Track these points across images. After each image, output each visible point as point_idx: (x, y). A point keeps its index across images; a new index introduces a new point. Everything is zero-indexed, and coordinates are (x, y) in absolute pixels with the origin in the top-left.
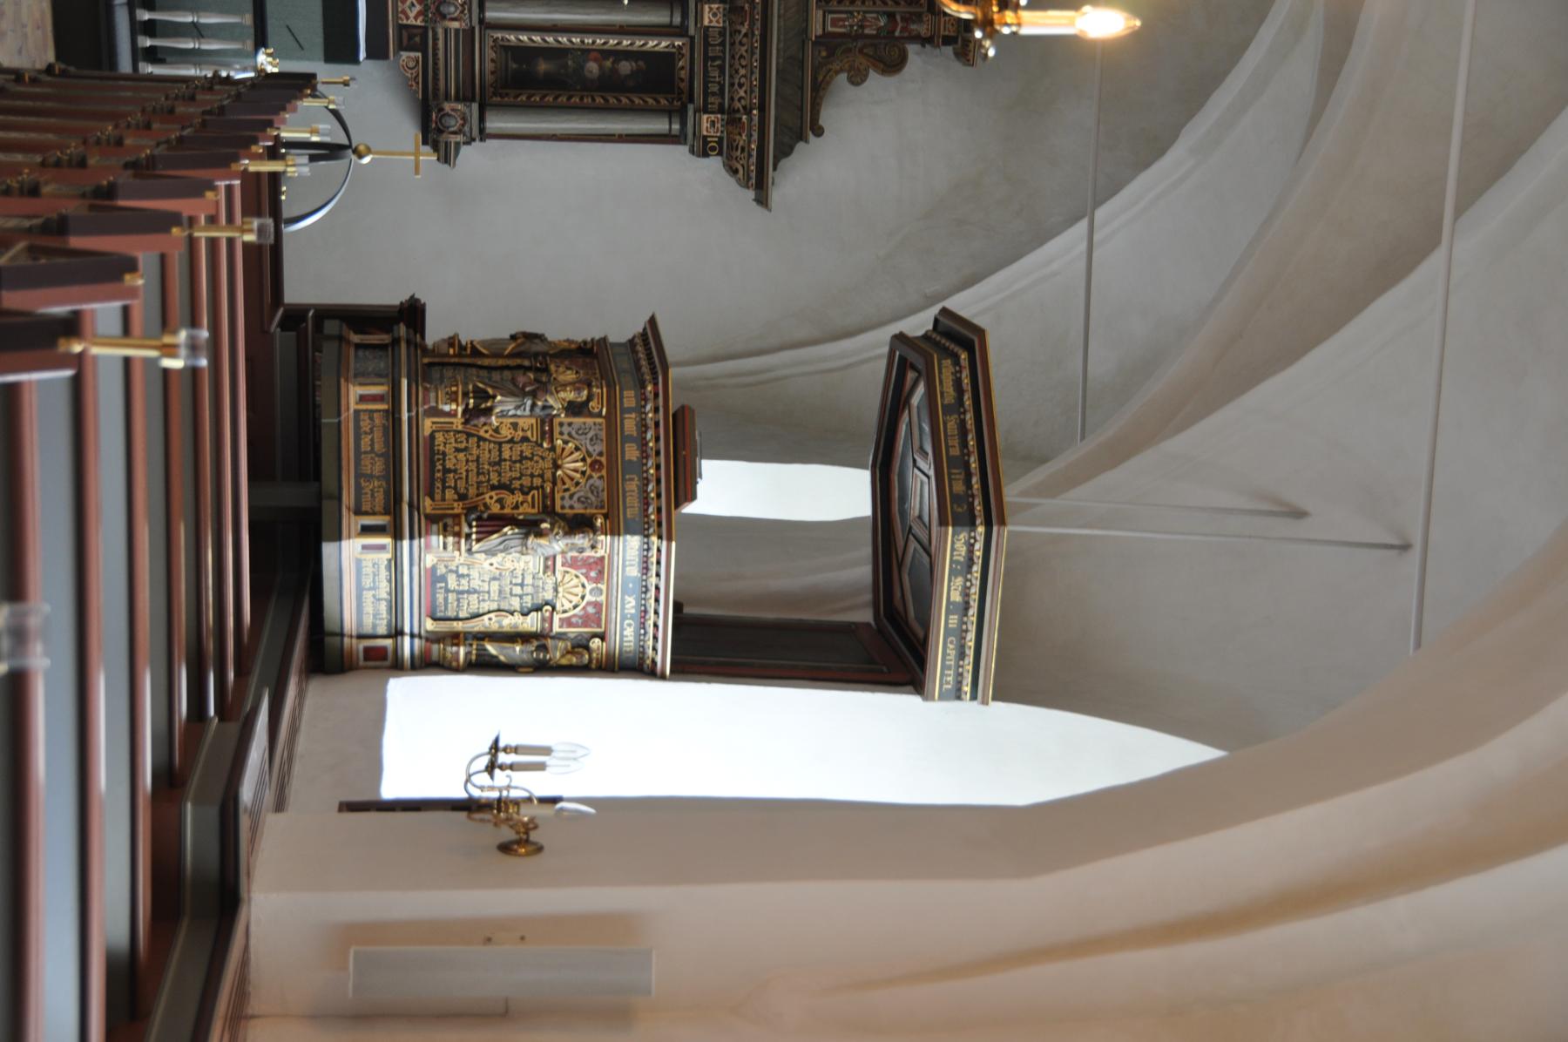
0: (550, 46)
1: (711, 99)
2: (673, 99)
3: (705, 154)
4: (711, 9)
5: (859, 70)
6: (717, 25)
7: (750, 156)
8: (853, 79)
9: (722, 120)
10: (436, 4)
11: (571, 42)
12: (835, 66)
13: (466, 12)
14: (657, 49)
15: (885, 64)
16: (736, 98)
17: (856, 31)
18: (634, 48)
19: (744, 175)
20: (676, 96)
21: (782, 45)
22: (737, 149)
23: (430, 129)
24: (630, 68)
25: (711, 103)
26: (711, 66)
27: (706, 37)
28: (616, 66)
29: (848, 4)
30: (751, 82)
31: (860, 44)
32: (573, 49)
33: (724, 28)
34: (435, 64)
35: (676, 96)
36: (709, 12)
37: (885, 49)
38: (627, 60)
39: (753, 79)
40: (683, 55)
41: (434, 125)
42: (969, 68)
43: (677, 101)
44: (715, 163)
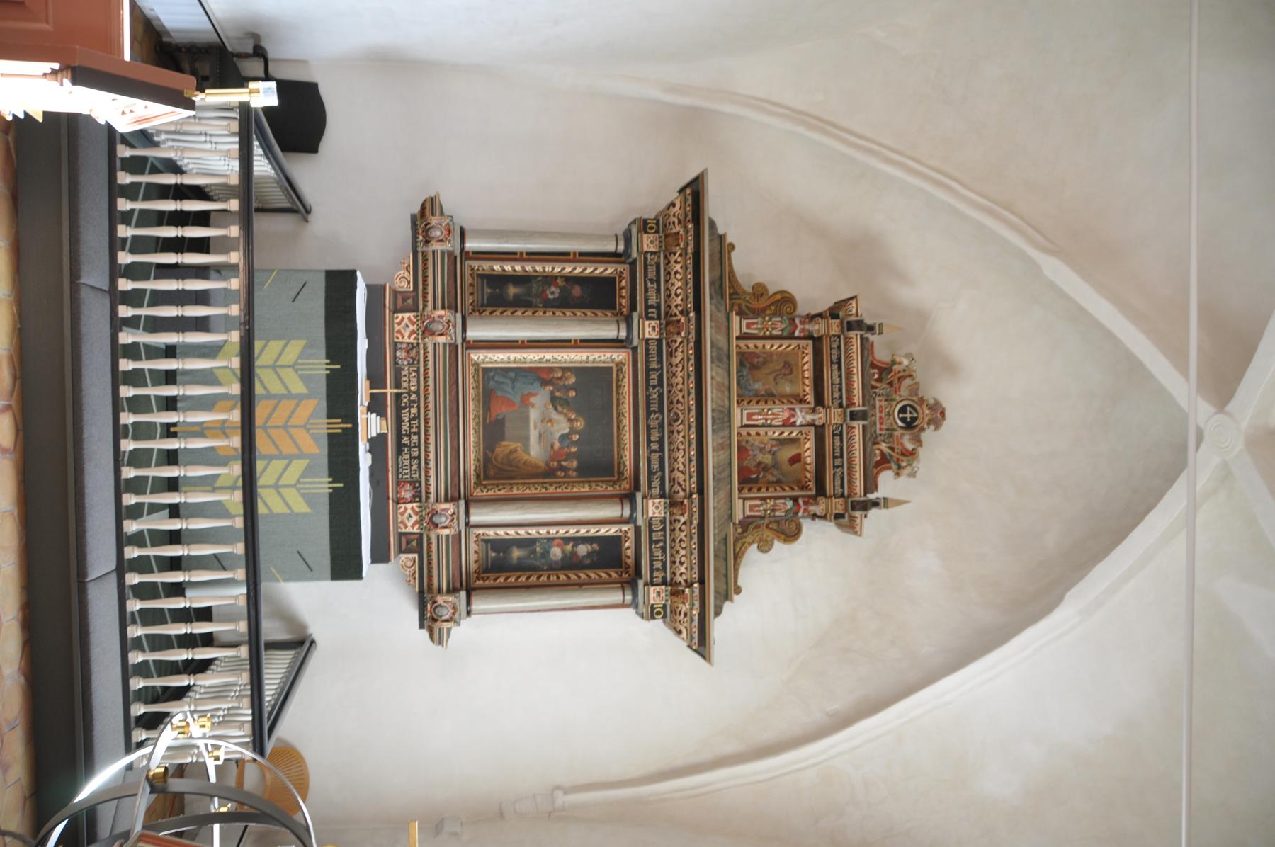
0: (522, 537)
1: (656, 574)
2: (622, 572)
3: (653, 618)
4: (654, 503)
5: (766, 541)
6: (659, 515)
7: (692, 620)
8: (762, 548)
9: (666, 591)
10: (430, 515)
11: (539, 533)
12: (749, 539)
13: (455, 520)
14: (607, 534)
15: (786, 535)
16: (678, 573)
17: (769, 514)
18: (590, 534)
19: (687, 635)
21: (716, 531)
22: (680, 614)
23: (425, 617)
24: (586, 550)
25: (656, 577)
26: (655, 548)
27: (650, 525)
28: (575, 549)
29: (756, 491)
30: (691, 561)
31: (766, 521)
32: (541, 538)
33: (665, 518)
34: (429, 563)
35: (623, 570)
36: (653, 506)
40: (629, 538)
41: (429, 615)
42: (850, 537)
43: (626, 574)
44: (659, 622)
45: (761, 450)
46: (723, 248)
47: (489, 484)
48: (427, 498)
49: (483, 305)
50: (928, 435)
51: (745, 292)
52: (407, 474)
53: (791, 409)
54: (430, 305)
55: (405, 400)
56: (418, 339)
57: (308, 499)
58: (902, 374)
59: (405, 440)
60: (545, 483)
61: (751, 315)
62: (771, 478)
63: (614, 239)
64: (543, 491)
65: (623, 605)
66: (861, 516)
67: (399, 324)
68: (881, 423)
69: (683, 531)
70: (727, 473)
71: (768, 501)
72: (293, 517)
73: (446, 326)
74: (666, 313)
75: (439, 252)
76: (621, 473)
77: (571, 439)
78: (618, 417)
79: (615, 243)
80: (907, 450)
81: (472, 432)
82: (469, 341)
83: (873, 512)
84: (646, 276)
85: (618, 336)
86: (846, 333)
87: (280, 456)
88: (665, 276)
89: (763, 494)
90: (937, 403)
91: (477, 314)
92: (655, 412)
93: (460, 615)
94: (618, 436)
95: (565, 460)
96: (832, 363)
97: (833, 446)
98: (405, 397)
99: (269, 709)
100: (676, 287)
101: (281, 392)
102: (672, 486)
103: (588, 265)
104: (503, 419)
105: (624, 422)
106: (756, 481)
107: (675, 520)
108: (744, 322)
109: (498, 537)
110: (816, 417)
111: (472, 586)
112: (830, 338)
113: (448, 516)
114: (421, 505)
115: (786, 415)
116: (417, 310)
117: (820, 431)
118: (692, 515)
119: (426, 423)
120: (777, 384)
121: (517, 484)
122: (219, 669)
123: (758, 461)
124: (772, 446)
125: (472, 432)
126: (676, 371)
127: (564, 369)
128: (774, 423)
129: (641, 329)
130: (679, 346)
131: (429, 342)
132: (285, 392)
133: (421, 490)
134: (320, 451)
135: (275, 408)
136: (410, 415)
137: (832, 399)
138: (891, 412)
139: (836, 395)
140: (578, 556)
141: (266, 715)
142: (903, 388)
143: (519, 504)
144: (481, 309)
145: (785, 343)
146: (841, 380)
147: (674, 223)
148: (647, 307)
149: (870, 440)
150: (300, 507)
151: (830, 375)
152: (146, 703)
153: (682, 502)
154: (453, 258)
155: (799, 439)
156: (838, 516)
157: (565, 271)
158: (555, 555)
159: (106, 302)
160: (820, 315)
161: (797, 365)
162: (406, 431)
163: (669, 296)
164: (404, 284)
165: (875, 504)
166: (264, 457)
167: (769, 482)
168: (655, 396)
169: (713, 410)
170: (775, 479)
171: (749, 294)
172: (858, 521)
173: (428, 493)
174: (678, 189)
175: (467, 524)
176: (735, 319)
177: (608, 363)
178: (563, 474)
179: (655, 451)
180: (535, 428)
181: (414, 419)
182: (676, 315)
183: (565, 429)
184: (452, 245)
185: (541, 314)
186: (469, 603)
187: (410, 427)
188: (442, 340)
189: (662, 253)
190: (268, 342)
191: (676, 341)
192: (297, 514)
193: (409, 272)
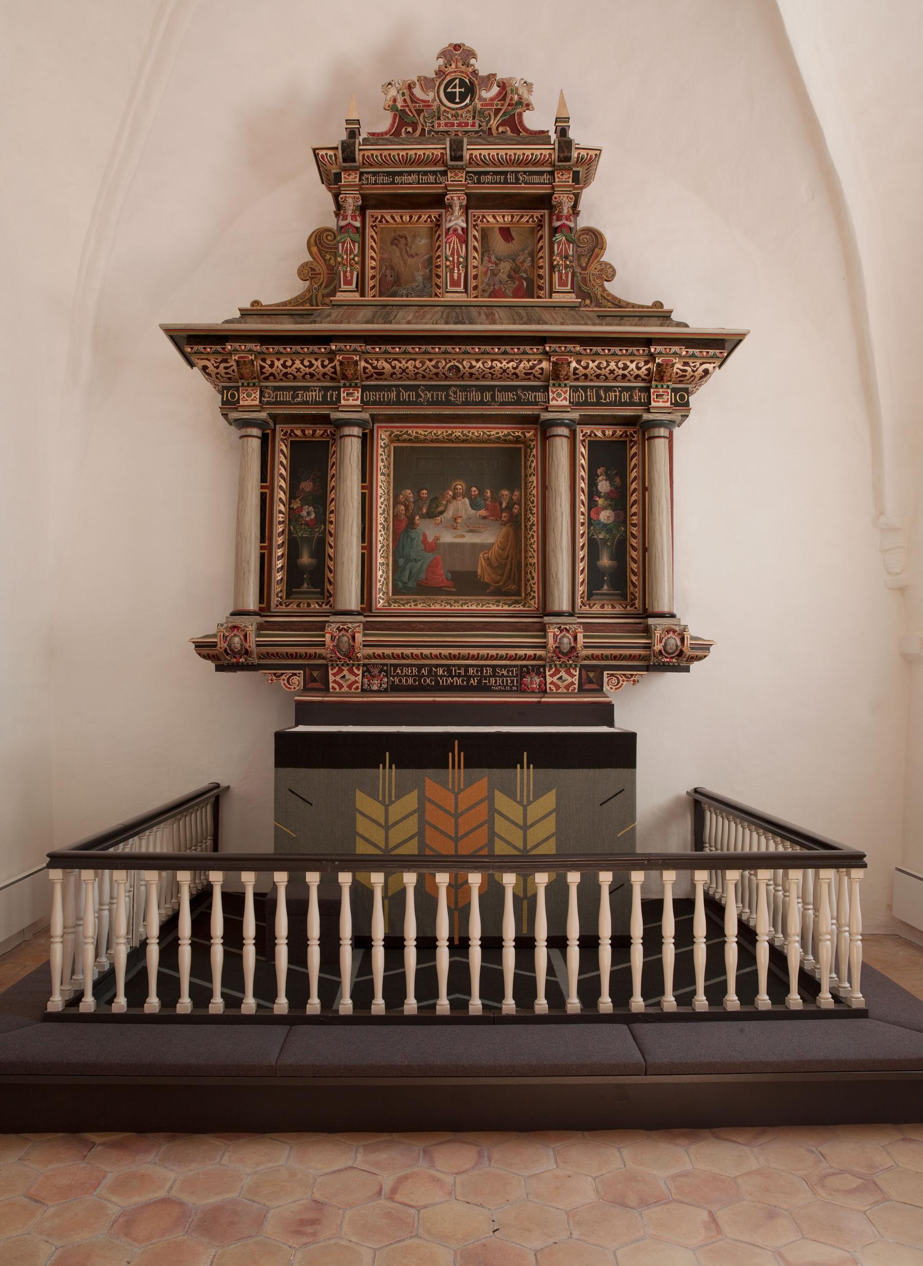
1: (636, 399)
3: (687, 404)
4: (554, 399)
5: (601, 270)
7: (693, 356)
9: (657, 387)
10: (560, 656)
11: (583, 535)
12: (599, 293)
15: (595, 247)
16: (636, 372)
18: (586, 477)
19: (710, 363)
20: (628, 439)
22: (686, 371)
26: (605, 400)
29: (542, 281)
31: (578, 270)
34: (615, 658)
37: (582, 247)
38: (597, 485)
39: (620, 353)
40: (592, 432)
45: (494, 274)
46: (254, 311)
47: (526, 589)
48: (540, 658)
49: (322, 593)
50: (483, 67)
51: (309, 290)
52: (512, 682)
53: (447, 234)
54: (319, 651)
55: (428, 681)
56: (359, 665)
57: (539, 793)
58: (407, 97)
59: (474, 682)
60: (526, 526)
61: (336, 282)
62: (528, 263)
63: (245, 439)
64: (535, 528)
65: (670, 438)
66: (577, 148)
67: (341, 686)
68: (467, 125)
69: (588, 364)
70: (521, 311)
71: (555, 263)
72: (560, 810)
73: (343, 632)
74: (332, 379)
75: (258, 639)
76: (517, 440)
77: (476, 496)
78: (453, 442)
79: (250, 439)
80: (499, 93)
81: (465, 607)
82: (362, 608)
83: (572, 134)
84: (289, 403)
85: (359, 437)
86: (357, 164)
87: (491, 822)
88: (288, 380)
89: (545, 272)
90: (443, 54)
91: (331, 599)
92: (447, 396)
93: (676, 625)
94: (474, 442)
95: (501, 504)
96: (393, 183)
97: (492, 183)
98: (425, 681)
99: (798, 848)
100: (301, 366)
101: (416, 820)
102: (534, 376)
103: (276, 472)
104: (452, 573)
105: (458, 434)
106: (530, 281)
107: (575, 374)
108: (343, 287)
109: (586, 581)
110: (457, 203)
111: (641, 612)
112: (363, 184)
113: (562, 634)
114: (548, 665)
115: (455, 239)
116: (327, 666)
117: (475, 202)
118: (570, 351)
119: (454, 657)
120: (417, 255)
121: (526, 558)
122: (720, 890)
123: (507, 279)
124: (490, 261)
125: (465, 607)
126: (400, 368)
127: (396, 502)
128: (463, 254)
129: (351, 409)
130: (371, 364)
131: (362, 652)
132: (416, 815)
133: (531, 665)
134: (484, 778)
135: (435, 827)
136: (445, 676)
137: (436, 183)
138: (453, 112)
139: (432, 178)
140: (611, 491)
141: (805, 851)
142: (425, 98)
143: (551, 554)
144: (327, 594)
145: (369, 242)
146: (414, 172)
147: (226, 368)
148: (324, 402)
149: (486, 135)
150: (549, 800)
151: (408, 186)
152: (787, 991)
153: (554, 363)
154: (265, 624)
155: (483, 229)
156: (576, 178)
157: (284, 499)
158: (608, 517)
159: (302, 1029)
160: (336, 197)
161: (395, 230)
162: (463, 681)
163: (312, 375)
164: (295, 679)
165: (563, 132)
166: (491, 844)
167: (533, 266)
168: (429, 395)
169: (447, 323)
170: (530, 259)
171: (311, 283)
172: (583, 153)
173: (535, 658)
174: (189, 367)
175: (571, 615)
176: (340, 296)
177: (389, 451)
178: (516, 506)
179: (493, 397)
180: (463, 536)
181: (450, 672)
182: (334, 367)
183: (465, 503)
184: (250, 624)
185: (332, 526)
186: (662, 615)
187: (459, 676)
188: (359, 638)
189: (262, 384)
190: (358, 834)
191: (365, 368)
192: (557, 804)
193: (282, 674)
